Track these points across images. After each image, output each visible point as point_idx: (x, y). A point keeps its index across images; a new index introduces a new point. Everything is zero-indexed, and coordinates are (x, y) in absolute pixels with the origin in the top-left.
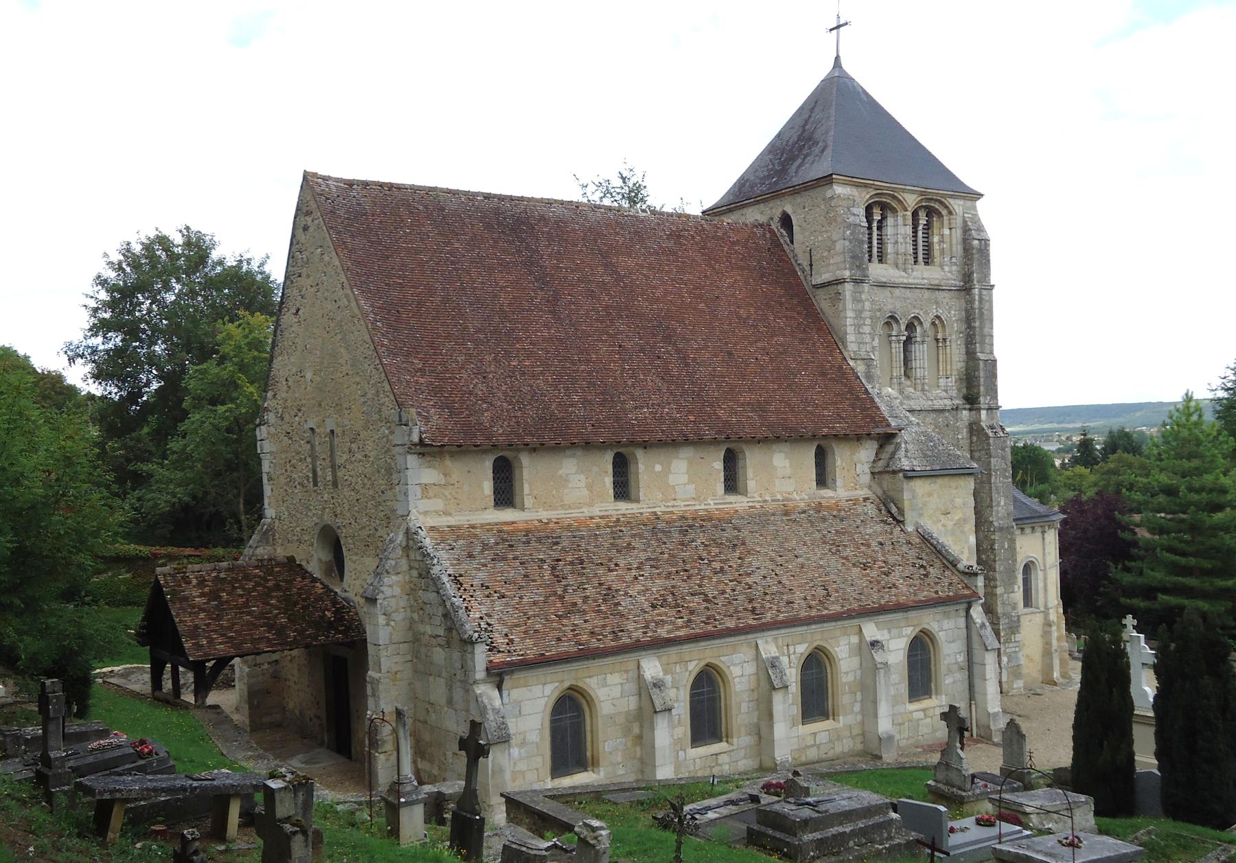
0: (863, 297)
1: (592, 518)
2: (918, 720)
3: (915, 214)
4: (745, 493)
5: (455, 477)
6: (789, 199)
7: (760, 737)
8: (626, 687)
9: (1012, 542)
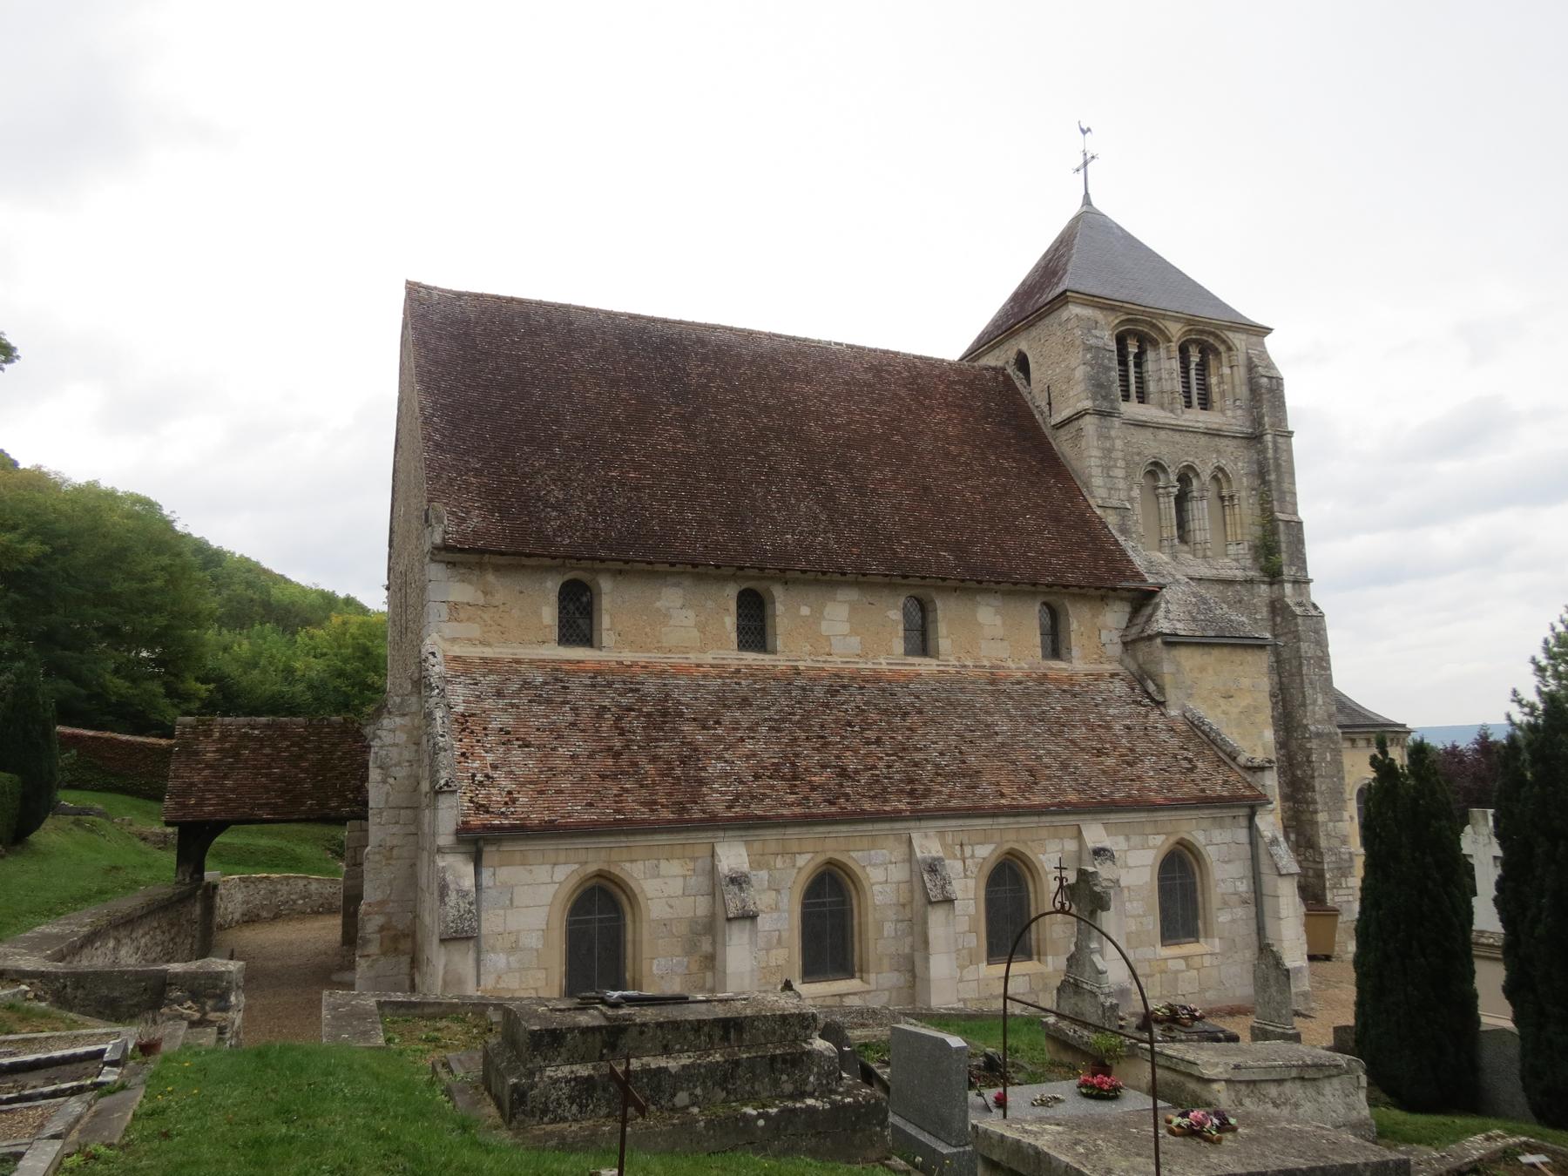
0: (1113, 433)
1: (698, 666)
2: (1177, 972)
3: (1184, 351)
4: (936, 655)
5: (499, 598)
6: (1024, 335)
7: (914, 976)
8: (692, 881)
9: (1337, 752)
